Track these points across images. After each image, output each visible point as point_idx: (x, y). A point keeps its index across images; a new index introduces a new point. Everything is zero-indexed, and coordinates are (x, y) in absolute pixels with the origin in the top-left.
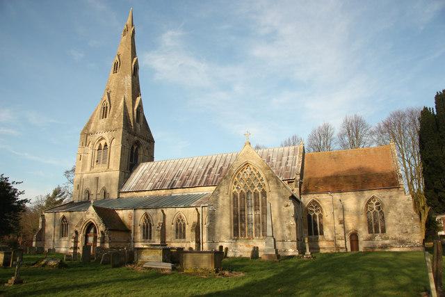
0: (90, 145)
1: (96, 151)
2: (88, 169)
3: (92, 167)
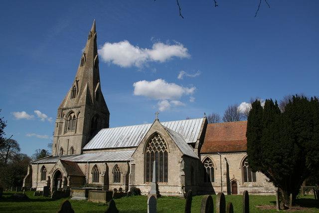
0: (64, 117)
1: (68, 122)
3: (65, 132)
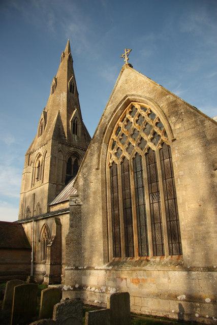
2: (29, 188)
3: (33, 185)
